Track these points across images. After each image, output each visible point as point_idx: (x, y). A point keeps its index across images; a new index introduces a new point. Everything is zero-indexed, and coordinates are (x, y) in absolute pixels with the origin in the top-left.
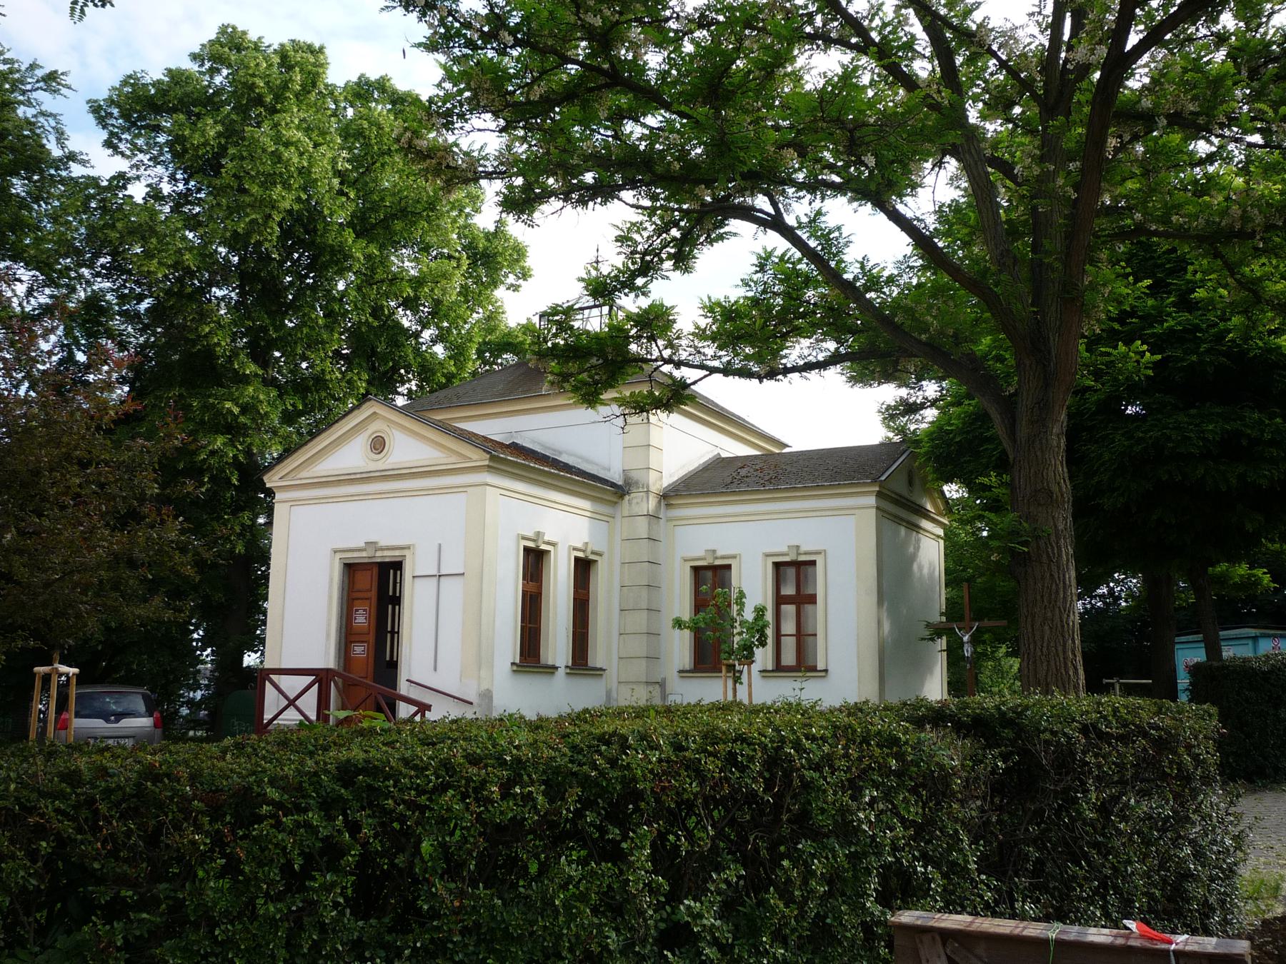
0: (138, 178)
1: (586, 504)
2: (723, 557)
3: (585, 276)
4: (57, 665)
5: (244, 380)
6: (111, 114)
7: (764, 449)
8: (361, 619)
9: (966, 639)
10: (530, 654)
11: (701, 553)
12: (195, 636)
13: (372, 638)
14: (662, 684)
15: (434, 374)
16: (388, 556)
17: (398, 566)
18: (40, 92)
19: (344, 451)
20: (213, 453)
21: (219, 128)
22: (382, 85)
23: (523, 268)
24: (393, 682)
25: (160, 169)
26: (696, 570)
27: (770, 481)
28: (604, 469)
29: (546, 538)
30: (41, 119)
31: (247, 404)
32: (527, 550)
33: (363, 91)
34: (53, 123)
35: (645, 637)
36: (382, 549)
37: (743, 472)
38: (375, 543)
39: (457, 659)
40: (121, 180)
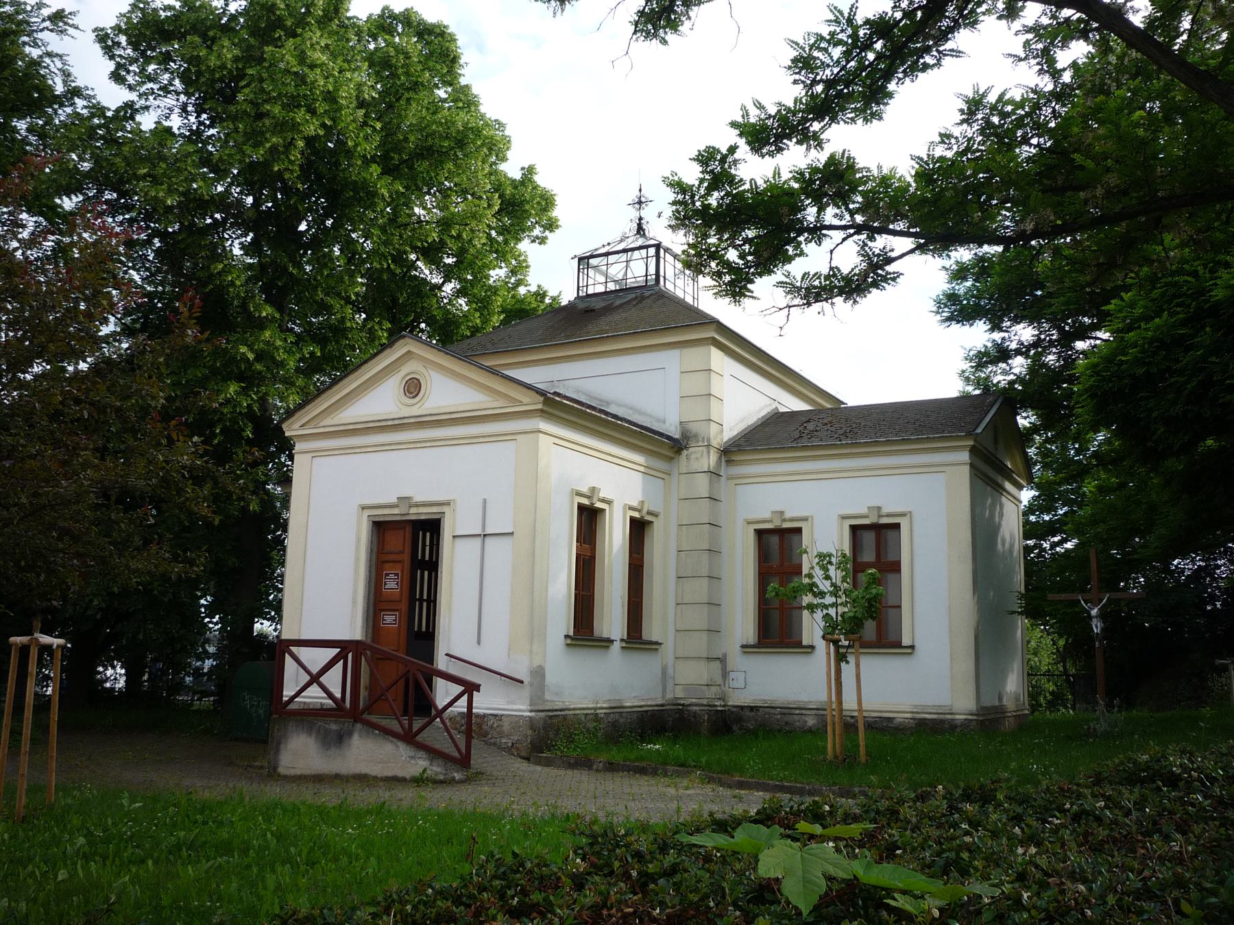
0: (147, 108)
1: (639, 458)
2: (792, 520)
3: (740, 120)
4: (37, 635)
5: (261, 324)
6: (118, 44)
7: (819, 404)
8: (391, 585)
9: (1094, 612)
10: (584, 629)
11: (767, 515)
12: (203, 602)
13: (404, 606)
14: (722, 660)
15: (458, 327)
16: (424, 513)
17: (433, 527)
18: (46, 32)
19: (376, 396)
20: (228, 401)
21: (237, 52)
22: (407, 19)
23: (550, 219)
24: (429, 655)
25: (170, 101)
26: (760, 533)
27: (845, 434)
28: (658, 420)
29: (602, 495)
30: (47, 60)
31: (262, 351)
32: (581, 508)
33: (385, 23)
34: (59, 65)
35: (706, 608)
36: (417, 505)
37: (811, 426)
38: (409, 498)
39: (502, 629)
40: (128, 111)
